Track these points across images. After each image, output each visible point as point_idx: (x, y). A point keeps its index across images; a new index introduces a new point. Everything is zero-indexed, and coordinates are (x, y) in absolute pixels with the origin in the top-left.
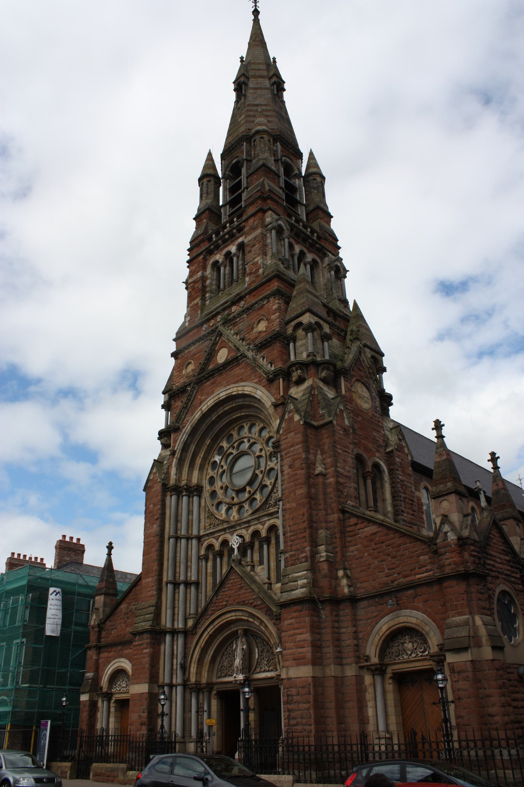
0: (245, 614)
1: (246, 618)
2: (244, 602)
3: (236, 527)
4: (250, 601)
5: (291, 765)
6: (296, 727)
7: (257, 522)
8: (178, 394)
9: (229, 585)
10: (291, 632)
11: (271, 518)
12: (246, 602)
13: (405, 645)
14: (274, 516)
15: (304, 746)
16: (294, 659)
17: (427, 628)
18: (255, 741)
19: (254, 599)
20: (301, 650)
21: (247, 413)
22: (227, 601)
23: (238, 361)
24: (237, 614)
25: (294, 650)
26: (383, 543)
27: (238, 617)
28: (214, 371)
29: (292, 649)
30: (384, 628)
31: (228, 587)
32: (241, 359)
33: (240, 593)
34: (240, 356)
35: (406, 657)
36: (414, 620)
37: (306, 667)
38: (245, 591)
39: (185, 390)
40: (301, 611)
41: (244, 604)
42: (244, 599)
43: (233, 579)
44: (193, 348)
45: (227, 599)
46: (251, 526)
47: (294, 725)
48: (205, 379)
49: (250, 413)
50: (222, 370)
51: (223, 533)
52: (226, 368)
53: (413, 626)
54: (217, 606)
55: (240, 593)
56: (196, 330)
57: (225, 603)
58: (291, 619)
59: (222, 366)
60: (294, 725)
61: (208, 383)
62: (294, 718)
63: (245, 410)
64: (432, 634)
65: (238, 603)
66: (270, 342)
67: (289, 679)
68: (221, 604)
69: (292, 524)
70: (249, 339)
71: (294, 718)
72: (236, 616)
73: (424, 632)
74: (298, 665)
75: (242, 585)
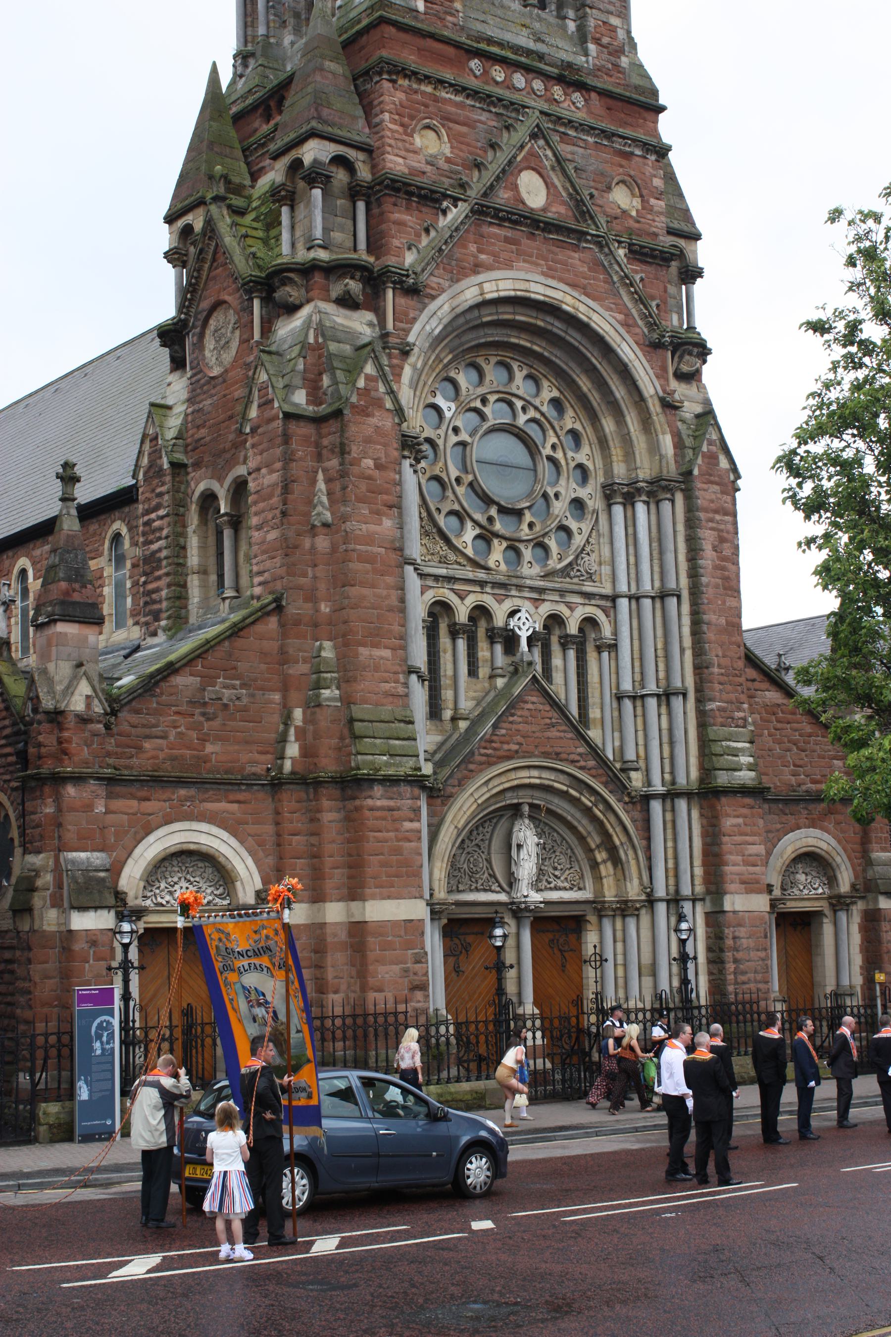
0: (562, 778)
1: (565, 788)
2: (557, 754)
3: (510, 590)
4: (572, 757)
5: (742, 1041)
6: (747, 986)
7: (557, 598)
8: (411, 194)
9: (526, 713)
10: (738, 839)
11: (587, 602)
12: (564, 756)
13: (798, 876)
14: (593, 602)
15: (759, 1014)
16: (743, 882)
17: (838, 859)
18: (706, 1007)
19: (580, 755)
20: (751, 869)
21: (546, 354)
22: (520, 744)
23: (579, 240)
24: (544, 776)
25: (744, 868)
26: (789, 723)
27: (546, 782)
28: (526, 218)
29: (739, 865)
30: (790, 850)
31: (521, 716)
32: (587, 241)
33: (549, 734)
34: (593, 235)
35: (797, 892)
36: (824, 846)
37: (760, 896)
38: (558, 734)
39: (438, 201)
40: (752, 807)
41: (557, 756)
42: (559, 750)
43: (533, 703)
44: (448, 96)
45: (519, 738)
46: (544, 600)
47: (744, 983)
48: (496, 216)
49: (554, 359)
50: (538, 228)
51: (478, 589)
52: (550, 232)
53: (823, 853)
54: (495, 749)
55: (549, 734)
56: (450, 51)
57: (515, 747)
58: (738, 817)
59: (546, 223)
60: (744, 983)
61: (495, 230)
62: (744, 973)
63: (544, 344)
64: (843, 868)
65: (546, 755)
66: (654, 257)
67: (734, 912)
68: (506, 747)
69: (720, 654)
70: (601, 206)
71: (744, 973)
72: (540, 778)
73: (834, 864)
74: (749, 891)
75: (554, 721)
